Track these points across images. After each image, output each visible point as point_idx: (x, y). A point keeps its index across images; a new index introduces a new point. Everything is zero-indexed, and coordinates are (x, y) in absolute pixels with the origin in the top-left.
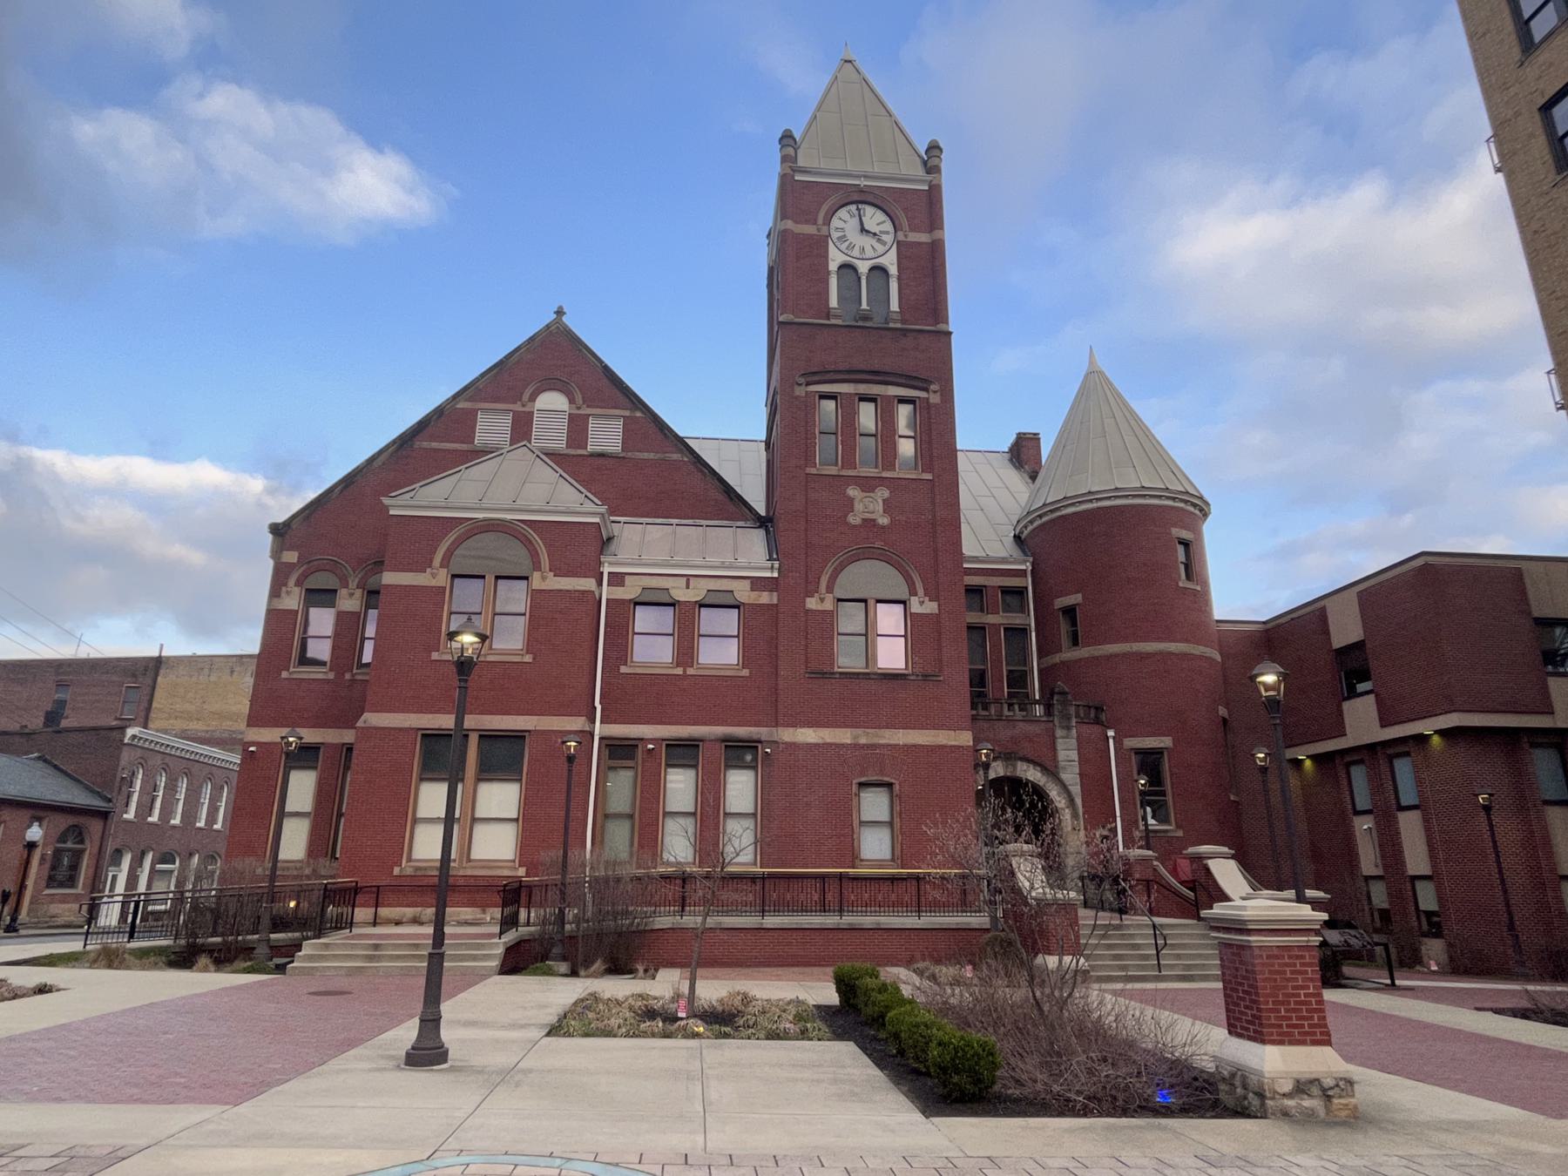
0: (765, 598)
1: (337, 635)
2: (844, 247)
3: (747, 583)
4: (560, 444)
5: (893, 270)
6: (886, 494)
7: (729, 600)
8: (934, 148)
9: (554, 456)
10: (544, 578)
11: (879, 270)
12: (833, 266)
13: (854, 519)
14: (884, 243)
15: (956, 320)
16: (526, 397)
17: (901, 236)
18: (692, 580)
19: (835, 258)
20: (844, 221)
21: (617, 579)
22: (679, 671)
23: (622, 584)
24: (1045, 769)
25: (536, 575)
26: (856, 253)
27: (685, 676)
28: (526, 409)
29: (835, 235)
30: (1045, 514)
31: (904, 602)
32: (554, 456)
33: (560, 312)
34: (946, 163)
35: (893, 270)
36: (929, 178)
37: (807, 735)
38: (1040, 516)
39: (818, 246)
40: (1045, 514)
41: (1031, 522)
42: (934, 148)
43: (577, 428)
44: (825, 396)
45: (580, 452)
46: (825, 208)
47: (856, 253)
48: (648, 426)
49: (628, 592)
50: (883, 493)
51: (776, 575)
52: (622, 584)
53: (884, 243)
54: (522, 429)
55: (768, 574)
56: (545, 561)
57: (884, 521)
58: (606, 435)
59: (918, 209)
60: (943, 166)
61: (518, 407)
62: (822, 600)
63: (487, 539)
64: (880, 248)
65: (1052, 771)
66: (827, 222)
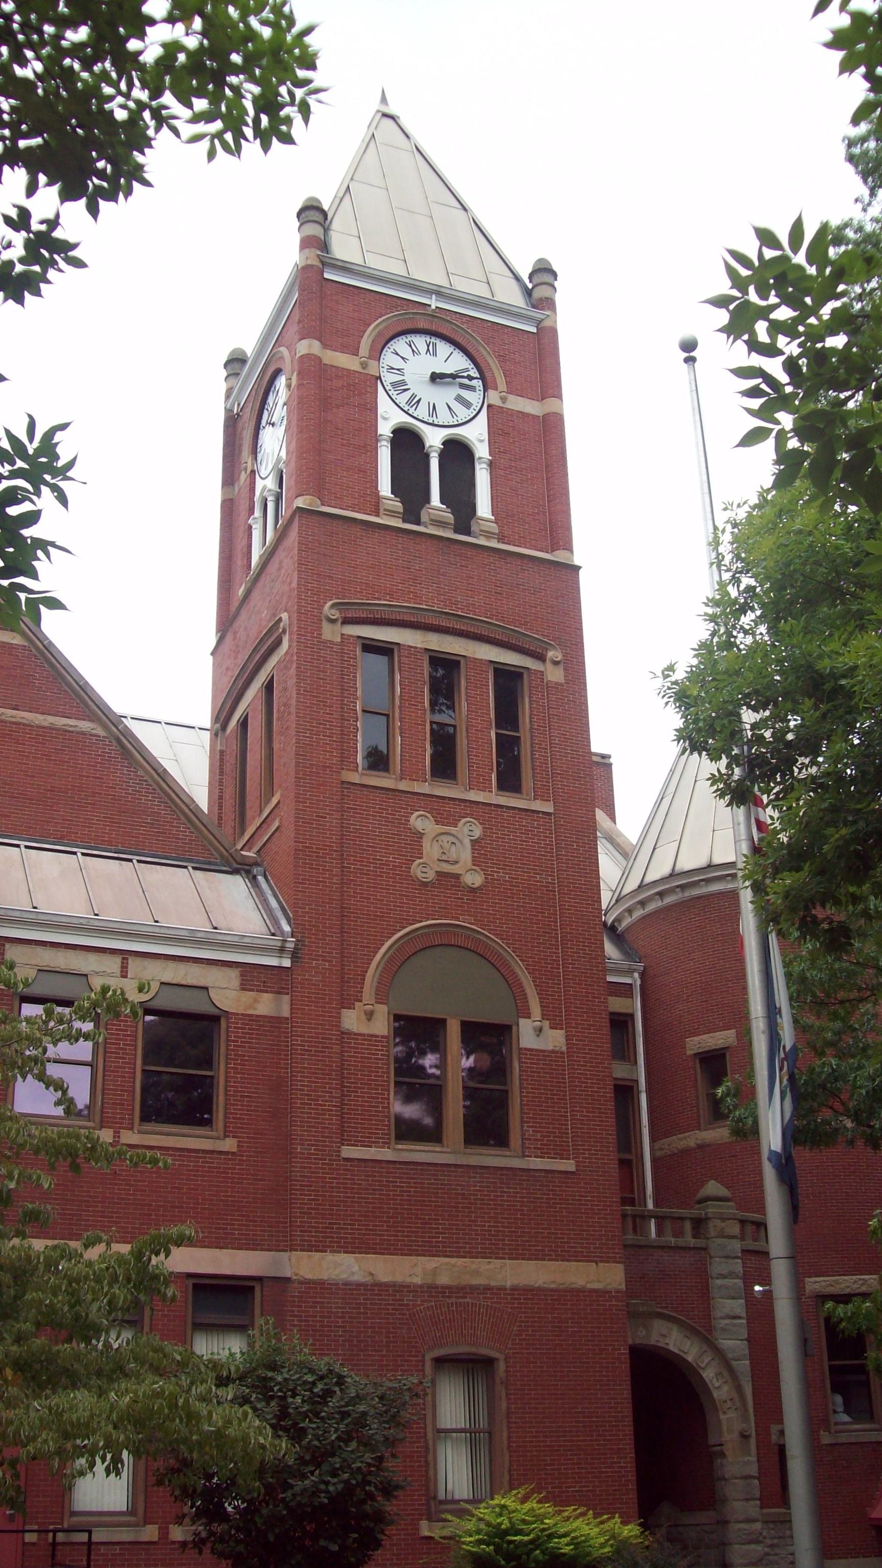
0: (265, 1005)
2: (403, 399)
3: (233, 975)
5: (482, 451)
8: (544, 271)
11: (457, 452)
12: (385, 429)
13: (423, 870)
14: (467, 404)
17: (494, 397)
18: (134, 965)
19: (389, 417)
20: (414, 362)
24: (692, 1331)
26: (422, 412)
29: (389, 378)
30: (671, 891)
34: (565, 295)
35: (482, 451)
36: (537, 314)
37: (344, 1267)
38: (661, 894)
39: (363, 389)
40: (671, 891)
41: (643, 903)
42: (544, 271)
44: (371, 647)
46: (370, 333)
47: (422, 412)
50: (470, 829)
51: (287, 963)
53: (467, 404)
55: (273, 961)
60: (559, 298)
62: (370, 1015)
64: (463, 413)
65: (703, 1330)
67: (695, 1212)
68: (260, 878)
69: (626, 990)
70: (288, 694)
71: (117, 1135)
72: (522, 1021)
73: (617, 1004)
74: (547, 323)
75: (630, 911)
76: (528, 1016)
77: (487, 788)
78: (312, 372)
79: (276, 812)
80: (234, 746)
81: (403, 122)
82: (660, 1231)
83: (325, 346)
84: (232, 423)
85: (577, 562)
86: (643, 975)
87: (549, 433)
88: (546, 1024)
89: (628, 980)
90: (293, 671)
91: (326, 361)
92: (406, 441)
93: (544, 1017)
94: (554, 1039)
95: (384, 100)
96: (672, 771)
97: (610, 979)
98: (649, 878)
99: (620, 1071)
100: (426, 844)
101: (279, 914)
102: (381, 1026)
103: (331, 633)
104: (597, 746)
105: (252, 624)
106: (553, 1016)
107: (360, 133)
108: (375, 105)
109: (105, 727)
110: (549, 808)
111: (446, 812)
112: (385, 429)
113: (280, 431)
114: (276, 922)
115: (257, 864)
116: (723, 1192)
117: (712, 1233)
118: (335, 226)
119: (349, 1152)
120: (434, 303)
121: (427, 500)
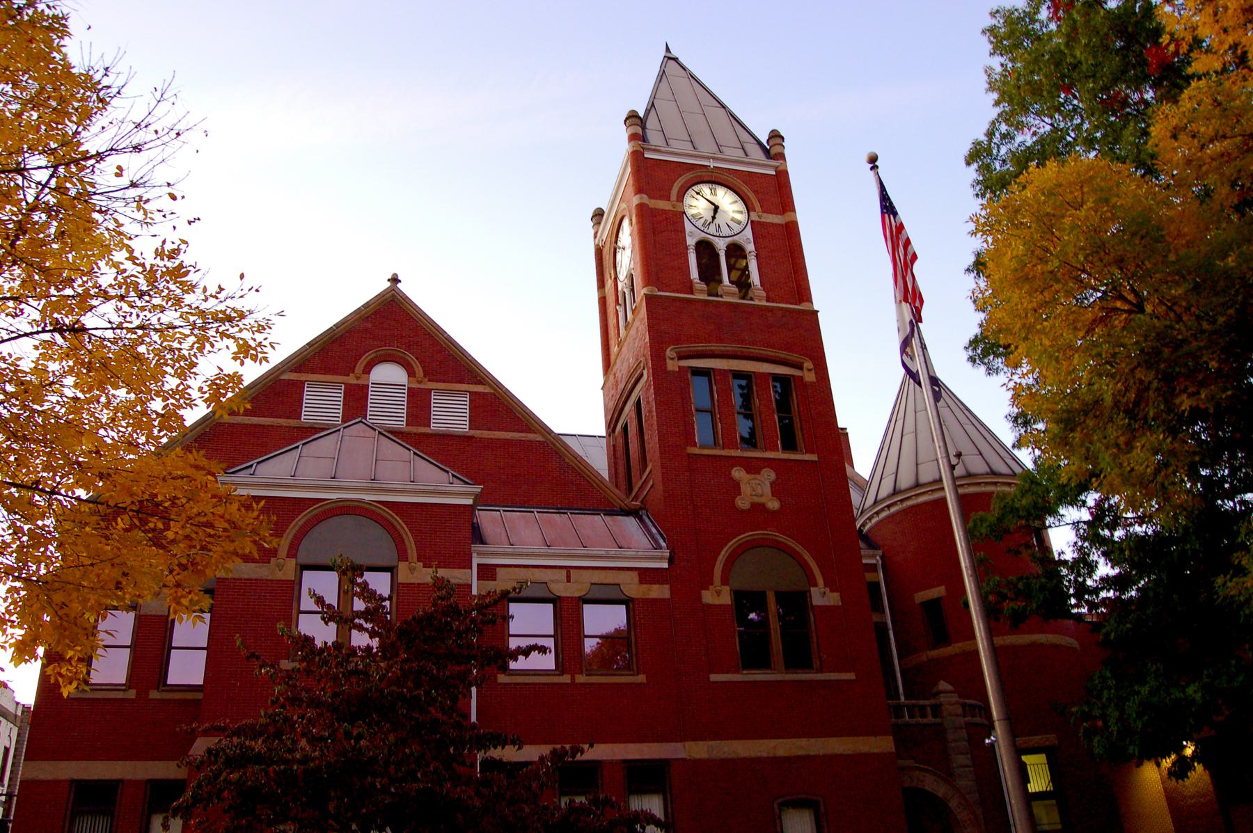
0: (660, 591)
1: (137, 646)
3: (635, 575)
4: (401, 423)
5: (750, 248)
6: (773, 476)
7: (614, 594)
9: (396, 435)
10: (412, 570)
11: (735, 251)
12: (691, 242)
13: (743, 503)
15: (820, 300)
16: (360, 366)
17: (754, 216)
21: (487, 572)
22: (566, 679)
23: (494, 578)
25: (402, 566)
27: (573, 685)
28: (360, 382)
31: (391, 569)
32: (396, 435)
33: (395, 280)
35: (750, 248)
38: (889, 507)
39: (677, 219)
41: (877, 513)
42: (775, 136)
43: (418, 404)
44: (697, 372)
45: (422, 430)
48: (496, 406)
49: (504, 582)
50: (768, 475)
51: (666, 565)
52: (494, 578)
54: (356, 403)
56: (412, 551)
57: (774, 505)
58: (451, 414)
59: (769, 190)
60: (786, 152)
61: (352, 380)
62: (718, 593)
63: (348, 521)
65: (947, 774)
66: (681, 198)
67: (932, 701)
68: (645, 517)
69: (873, 568)
70: (649, 407)
71: (573, 678)
72: (812, 589)
73: (869, 577)
74: (781, 168)
75: (870, 519)
76: (815, 585)
77: (775, 449)
78: (644, 213)
79: (652, 478)
80: (621, 441)
81: (681, 60)
82: (911, 716)
83: (651, 197)
84: (599, 253)
85: (816, 308)
86: (882, 558)
87: (791, 232)
88: (828, 590)
89: (873, 561)
90: (652, 391)
91: (651, 206)
92: (705, 248)
93: (826, 585)
94: (833, 599)
95: (668, 49)
96: (886, 432)
97: (864, 561)
98: (880, 497)
99: (876, 618)
100: (742, 486)
101: (658, 537)
102: (726, 598)
103: (672, 365)
104: (840, 425)
105: (622, 368)
106: (831, 585)
107: (656, 70)
108: (663, 53)
109: (543, 436)
110: (814, 457)
111: (753, 467)
112: (691, 242)
113: (628, 252)
114: (656, 541)
115: (641, 508)
116: (950, 687)
117: (945, 714)
118: (648, 125)
119: (714, 677)
120: (712, 164)
121: (721, 281)
